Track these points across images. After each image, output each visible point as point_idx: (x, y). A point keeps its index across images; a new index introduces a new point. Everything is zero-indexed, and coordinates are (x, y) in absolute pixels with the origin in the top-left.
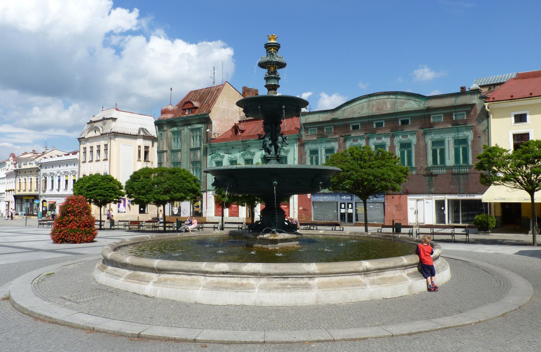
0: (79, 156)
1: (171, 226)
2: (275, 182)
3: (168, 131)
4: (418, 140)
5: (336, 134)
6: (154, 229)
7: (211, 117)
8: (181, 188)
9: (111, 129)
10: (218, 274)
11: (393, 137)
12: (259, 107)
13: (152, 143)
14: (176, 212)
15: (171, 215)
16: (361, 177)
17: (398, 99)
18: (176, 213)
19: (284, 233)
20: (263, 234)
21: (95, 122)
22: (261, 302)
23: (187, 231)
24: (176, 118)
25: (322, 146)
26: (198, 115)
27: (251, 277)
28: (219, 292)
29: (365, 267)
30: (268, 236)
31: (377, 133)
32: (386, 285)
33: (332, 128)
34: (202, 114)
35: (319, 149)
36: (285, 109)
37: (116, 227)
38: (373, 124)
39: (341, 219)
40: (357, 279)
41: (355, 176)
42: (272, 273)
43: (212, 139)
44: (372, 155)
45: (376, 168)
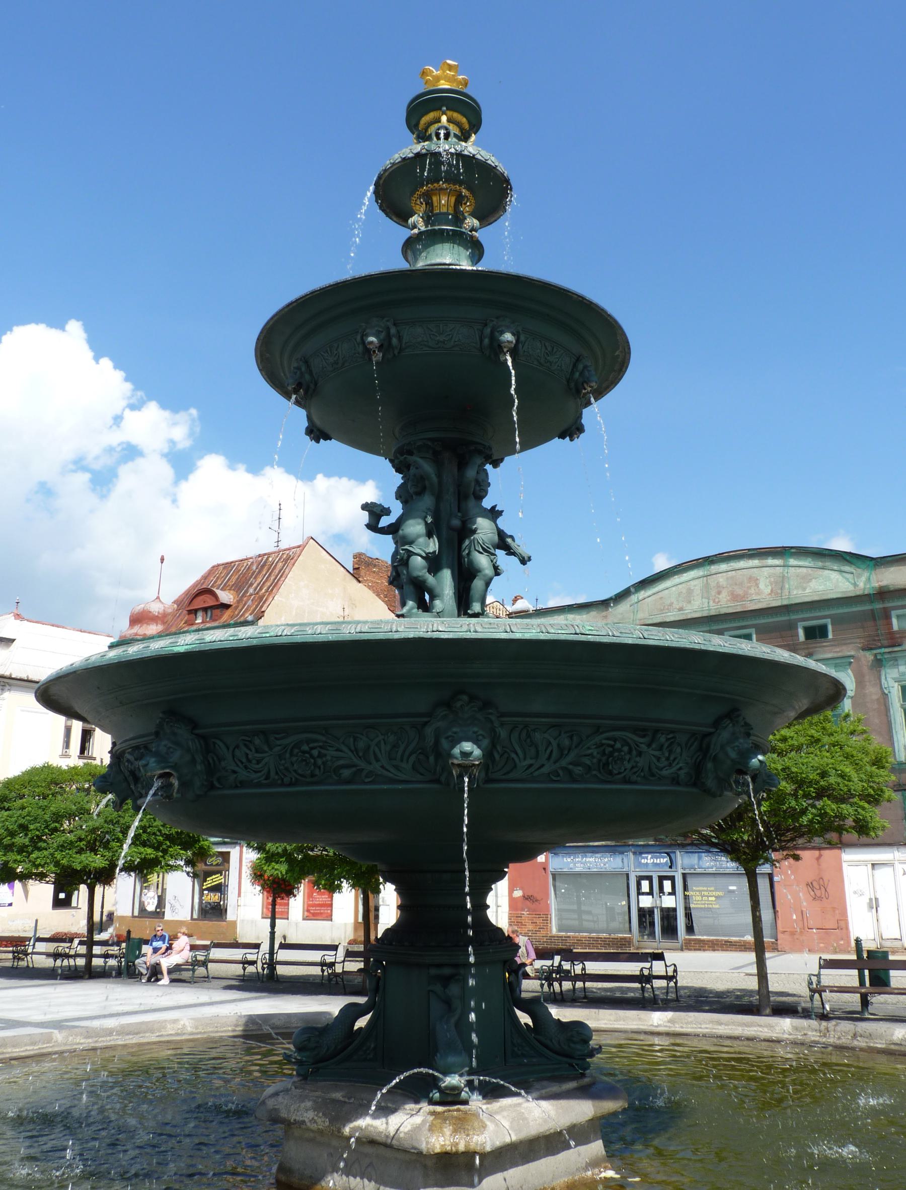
2: (467, 746)
4: (860, 683)
8: (144, 832)
12: (372, 339)
14: (151, 907)
15: (136, 913)
18: (151, 907)
19: (517, 1095)
20: (385, 1110)
23: (155, 973)
30: (417, 1129)
34: (239, 621)
45: (793, 753)
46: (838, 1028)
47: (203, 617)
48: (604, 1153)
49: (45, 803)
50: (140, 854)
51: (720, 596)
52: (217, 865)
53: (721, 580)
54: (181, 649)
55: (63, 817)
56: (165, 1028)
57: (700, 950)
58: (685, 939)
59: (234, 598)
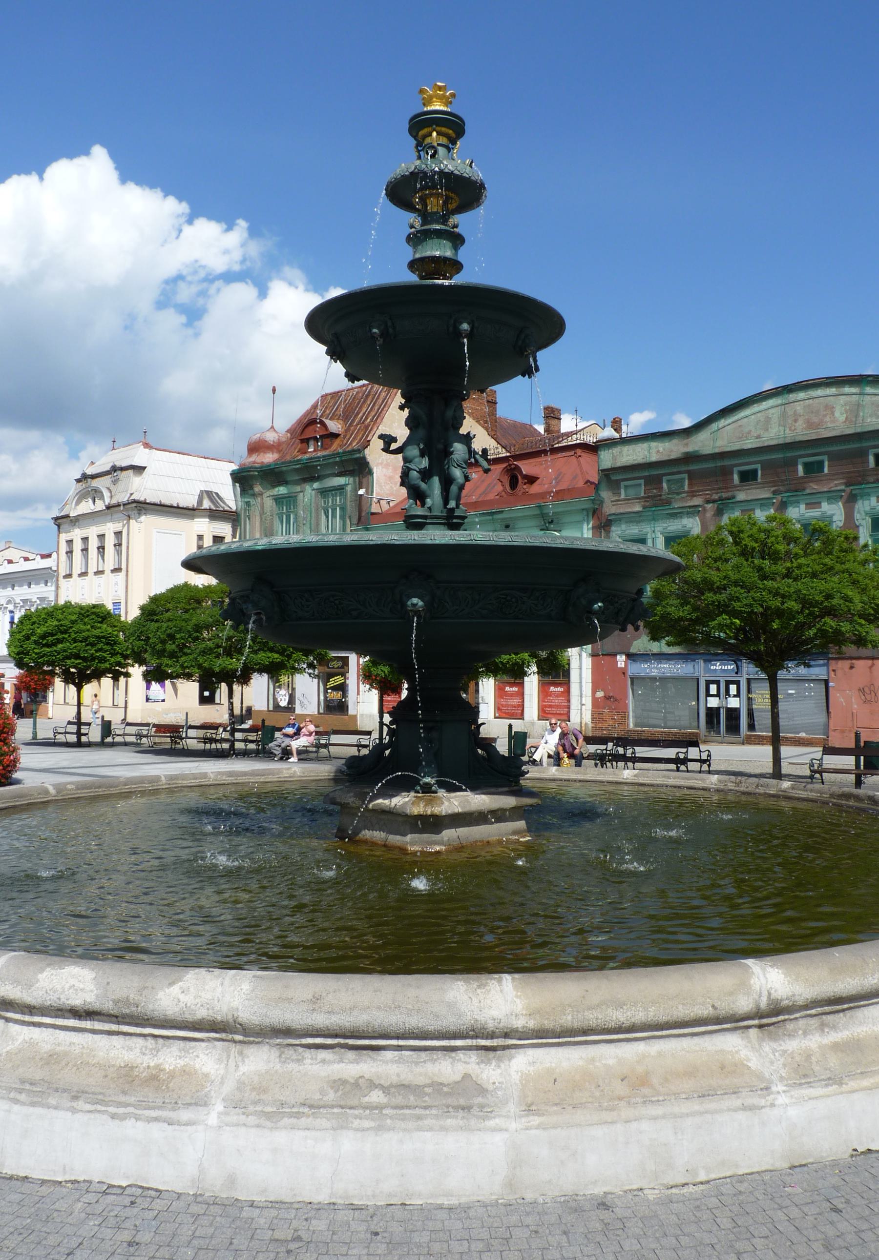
0: (55, 563)
1: (250, 738)
2: (415, 600)
3: (265, 495)
5: (694, 496)
6: (208, 746)
7: (369, 458)
9: (132, 494)
10: (56, 1017)
11: (851, 500)
12: (375, 330)
13: (231, 529)
14: (283, 703)
15: (271, 708)
16: (762, 606)
17: (866, 396)
18: (283, 703)
21: (94, 477)
22: (231, 1181)
23: (286, 753)
24: (283, 463)
25: (657, 529)
26: (338, 453)
27: (202, 1040)
28: (39, 1110)
29: (765, 994)
30: (406, 803)
31: (808, 491)
32: (866, 1083)
33: (684, 479)
34: (347, 450)
35: (649, 536)
36: (470, 335)
37: (118, 739)
38: (797, 465)
39: (707, 723)
40: (722, 1051)
41: (745, 602)
42: (294, 1026)
43: (373, 514)
44: (796, 540)
46: (748, 781)
47: (314, 446)
48: (525, 828)
49: (187, 616)
50: (268, 658)
51: (797, 424)
52: (338, 668)
53: (798, 408)
54: (260, 548)
55: (202, 628)
56: (282, 772)
57: (759, 744)
58: (747, 735)
59: (342, 428)
